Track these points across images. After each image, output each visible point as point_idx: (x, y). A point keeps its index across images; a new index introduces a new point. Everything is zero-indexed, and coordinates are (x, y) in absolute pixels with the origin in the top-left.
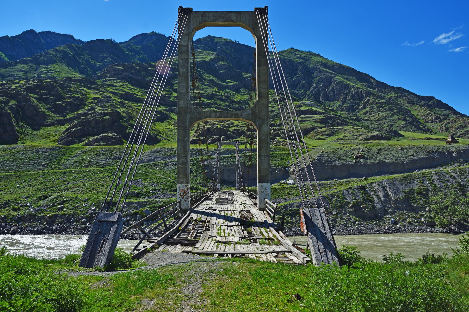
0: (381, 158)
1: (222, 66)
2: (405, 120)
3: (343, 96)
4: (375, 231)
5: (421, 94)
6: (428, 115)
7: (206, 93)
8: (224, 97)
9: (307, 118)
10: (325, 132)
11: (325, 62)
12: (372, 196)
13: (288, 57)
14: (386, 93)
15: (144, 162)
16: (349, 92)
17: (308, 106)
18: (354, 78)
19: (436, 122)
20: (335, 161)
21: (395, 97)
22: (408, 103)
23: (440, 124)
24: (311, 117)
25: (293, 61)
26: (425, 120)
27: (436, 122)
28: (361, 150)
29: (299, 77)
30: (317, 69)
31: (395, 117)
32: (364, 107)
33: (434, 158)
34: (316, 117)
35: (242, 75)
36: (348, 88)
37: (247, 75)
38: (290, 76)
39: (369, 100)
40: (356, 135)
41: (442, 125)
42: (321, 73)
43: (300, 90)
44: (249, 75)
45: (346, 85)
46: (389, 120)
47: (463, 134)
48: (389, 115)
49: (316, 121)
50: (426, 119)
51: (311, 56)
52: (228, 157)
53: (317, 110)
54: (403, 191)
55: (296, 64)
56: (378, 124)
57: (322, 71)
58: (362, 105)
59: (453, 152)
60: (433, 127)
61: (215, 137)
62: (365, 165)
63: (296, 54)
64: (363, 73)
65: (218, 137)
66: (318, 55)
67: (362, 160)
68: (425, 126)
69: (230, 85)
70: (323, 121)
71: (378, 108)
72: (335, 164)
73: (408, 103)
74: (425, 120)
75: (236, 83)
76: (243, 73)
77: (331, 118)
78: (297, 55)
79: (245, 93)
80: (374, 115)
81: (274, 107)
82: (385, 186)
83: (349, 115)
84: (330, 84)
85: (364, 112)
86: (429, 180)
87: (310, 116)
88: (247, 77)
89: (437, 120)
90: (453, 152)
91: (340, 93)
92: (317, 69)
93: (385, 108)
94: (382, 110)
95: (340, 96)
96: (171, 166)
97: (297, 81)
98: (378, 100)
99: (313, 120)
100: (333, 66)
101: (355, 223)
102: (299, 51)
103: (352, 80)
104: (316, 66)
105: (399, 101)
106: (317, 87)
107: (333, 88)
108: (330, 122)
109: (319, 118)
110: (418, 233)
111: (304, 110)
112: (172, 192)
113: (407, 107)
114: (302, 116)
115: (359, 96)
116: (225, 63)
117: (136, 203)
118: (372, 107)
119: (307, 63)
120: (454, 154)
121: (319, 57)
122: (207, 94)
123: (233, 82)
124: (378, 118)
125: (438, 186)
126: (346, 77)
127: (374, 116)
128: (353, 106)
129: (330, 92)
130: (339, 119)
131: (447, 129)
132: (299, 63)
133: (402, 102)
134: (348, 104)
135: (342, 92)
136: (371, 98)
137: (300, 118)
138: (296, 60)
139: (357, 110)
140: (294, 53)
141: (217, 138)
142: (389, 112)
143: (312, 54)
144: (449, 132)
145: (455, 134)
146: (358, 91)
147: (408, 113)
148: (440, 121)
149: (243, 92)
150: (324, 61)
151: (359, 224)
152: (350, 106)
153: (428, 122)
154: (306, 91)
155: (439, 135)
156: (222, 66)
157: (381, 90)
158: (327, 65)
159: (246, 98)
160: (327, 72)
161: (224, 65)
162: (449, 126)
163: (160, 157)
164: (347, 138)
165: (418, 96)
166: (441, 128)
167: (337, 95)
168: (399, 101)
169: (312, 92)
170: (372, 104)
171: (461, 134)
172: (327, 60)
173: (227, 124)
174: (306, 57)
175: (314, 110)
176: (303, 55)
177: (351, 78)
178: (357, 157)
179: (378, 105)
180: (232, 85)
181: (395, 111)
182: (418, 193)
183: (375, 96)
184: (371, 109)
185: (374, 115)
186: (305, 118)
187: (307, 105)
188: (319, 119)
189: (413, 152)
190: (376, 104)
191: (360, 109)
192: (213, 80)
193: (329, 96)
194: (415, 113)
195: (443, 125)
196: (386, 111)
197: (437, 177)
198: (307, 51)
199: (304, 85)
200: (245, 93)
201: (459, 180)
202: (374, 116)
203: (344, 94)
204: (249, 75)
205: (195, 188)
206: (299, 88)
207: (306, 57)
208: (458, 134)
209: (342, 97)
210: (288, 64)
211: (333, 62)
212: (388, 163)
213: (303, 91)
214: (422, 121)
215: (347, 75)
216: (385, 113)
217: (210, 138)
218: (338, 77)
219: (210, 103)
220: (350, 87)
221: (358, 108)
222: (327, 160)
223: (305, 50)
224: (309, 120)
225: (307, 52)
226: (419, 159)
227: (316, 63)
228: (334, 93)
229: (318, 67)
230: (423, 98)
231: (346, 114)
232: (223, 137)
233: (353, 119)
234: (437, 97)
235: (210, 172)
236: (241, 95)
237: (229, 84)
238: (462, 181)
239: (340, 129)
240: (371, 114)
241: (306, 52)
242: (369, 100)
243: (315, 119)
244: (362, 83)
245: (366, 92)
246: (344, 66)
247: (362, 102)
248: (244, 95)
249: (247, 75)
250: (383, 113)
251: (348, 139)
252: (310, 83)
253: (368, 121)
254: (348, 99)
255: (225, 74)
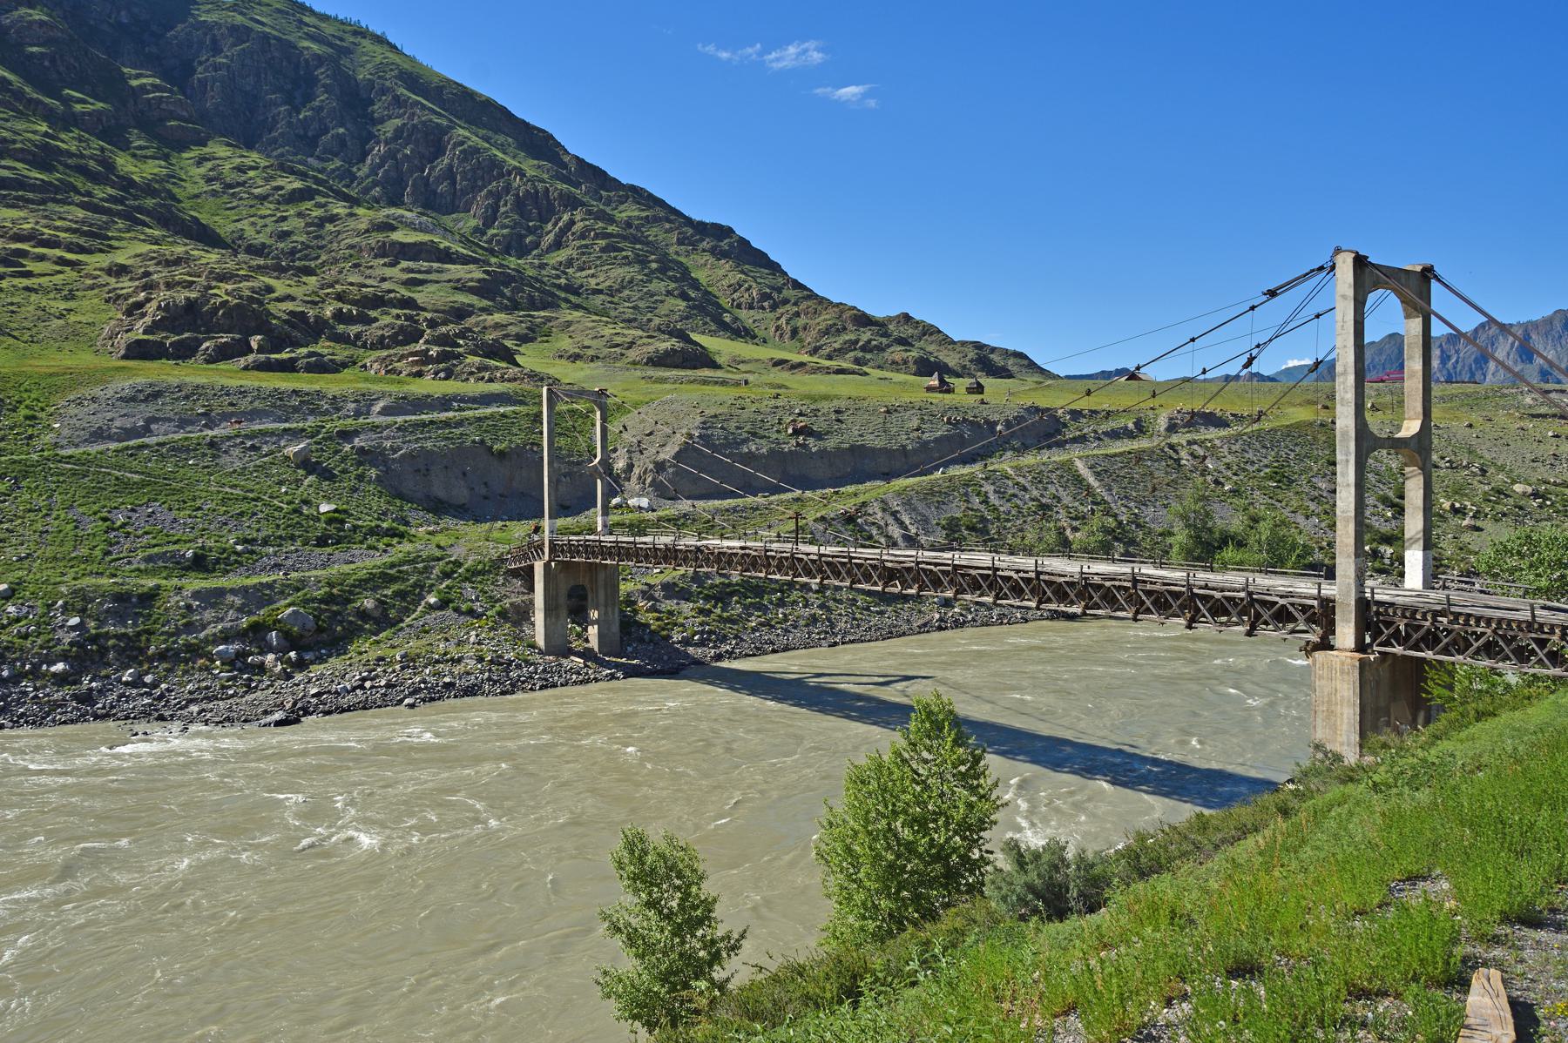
0: (854, 433)
1: (35, 27)
2: (684, 296)
3: (487, 197)
4: (919, 627)
5: (696, 216)
6: (741, 286)
7: (19, 138)
8: (92, 163)
9: (428, 272)
10: (506, 326)
11: (410, 69)
12: (877, 538)
13: (273, 28)
14: (614, 205)
15: (110, 438)
16: (507, 189)
17: (415, 230)
18: (510, 140)
19: (763, 308)
20: (745, 441)
21: (639, 218)
22: (680, 242)
23: (771, 315)
24: (439, 271)
25: (295, 47)
26: (733, 300)
27: (763, 308)
28: (797, 411)
29: (321, 108)
30: (384, 91)
31: (657, 286)
32: (558, 245)
33: (962, 436)
34: (456, 271)
35: (123, 79)
36: (501, 175)
37: (144, 81)
38: (285, 103)
39: (572, 223)
40: (617, 345)
41: (778, 319)
42: (400, 108)
43: (328, 160)
44: (150, 80)
45: (494, 164)
46: (641, 294)
47: (839, 350)
48: (640, 277)
49: (460, 286)
50: (736, 296)
51: (358, 39)
52: (424, 425)
53: (449, 248)
54: (938, 524)
55: (307, 61)
56: (633, 308)
57: (406, 101)
58: (551, 237)
59: (996, 423)
60: (754, 321)
61: (225, 338)
62: (823, 453)
63: (301, 22)
64: (535, 128)
65: (237, 336)
66: (380, 40)
67: (811, 441)
68: (736, 319)
69: (84, 114)
70: (482, 290)
71: (603, 250)
72: (750, 451)
73: (680, 242)
74: (733, 300)
75: (101, 105)
76: (125, 70)
77: (507, 279)
78: (308, 25)
79: (149, 152)
80: (592, 271)
81: (284, 219)
82: (897, 512)
83: (544, 272)
84: (439, 151)
85: (559, 259)
86: (978, 494)
87: (435, 265)
88: (142, 87)
89: (766, 304)
90: (996, 423)
91: (475, 189)
92: (384, 91)
93: (624, 253)
94: (615, 258)
95: (474, 198)
96: (236, 452)
97: (315, 125)
98: (601, 224)
99: (450, 281)
100: (440, 89)
101: (868, 609)
102: (312, 12)
103: (502, 145)
104: (380, 77)
105: (653, 233)
106: (391, 155)
107: (450, 166)
108: (507, 291)
109: (469, 276)
110: (1001, 623)
111: (409, 244)
112: (314, 546)
113: (677, 253)
114: (404, 264)
115: (537, 207)
116: (45, 18)
117: (233, 591)
118: (586, 246)
119: (344, 61)
120: (999, 428)
121: (386, 47)
122: (22, 142)
123: (91, 100)
124: (608, 283)
125: (1002, 509)
126: (482, 132)
127: (593, 276)
128: (523, 237)
129: (439, 180)
130: (532, 286)
131: (794, 332)
132: (320, 60)
133: (660, 238)
134: (506, 227)
135: (480, 183)
136: (578, 215)
137: (403, 270)
138: (306, 44)
139: (535, 252)
140: (293, 15)
141: (233, 339)
142: (637, 267)
143: (362, 33)
144: (801, 341)
145: (820, 347)
146: (535, 188)
147: (685, 275)
148: (774, 308)
149: (140, 148)
150: (406, 66)
151: (878, 613)
152: (510, 235)
153: (739, 306)
154: (351, 164)
155: (775, 347)
156: (35, 27)
157: (596, 192)
158: (415, 79)
159: (156, 170)
160: (424, 107)
161: (42, 23)
162: (801, 322)
163: (169, 420)
164: (590, 352)
165: (689, 221)
166: (778, 328)
167: (464, 192)
168: (653, 233)
169: (374, 171)
170: (583, 236)
171: (835, 350)
172: (412, 60)
173: (253, 290)
174: (341, 39)
175: (442, 246)
176: (328, 29)
177: (501, 139)
178: (796, 432)
179: (602, 243)
180: (89, 114)
181: (654, 266)
182: (968, 528)
183: (589, 213)
184: (583, 253)
185: (592, 271)
186: (420, 272)
187: (411, 226)
188: (471, 280)
189: (915, 423)
190: (597, 236)
191: (545, 248)
192: (10, 83)
193: (435, 192)
194: (701, 275)
195: (783, 320)
196: (629, 264)
197: (992, 488)
198: (340, 17)
199: (342, 141)
200: (149, 152)
201: (1035, 493)
202: (593, 276)
203: (490, 192)
204: (150, 80)
205: (388, 529)
206: (325, 151)
207: (341, 39)
208: (828, 350)
209: (481, 201)
210: (276, 54)
211: (438, 75)
212: (873, 450)
213: (338, 163)
214: (725, 302)
215: (484, 126)
216: (627, 269)
217: (206, 340)
218: (461, 131)
219: (50, 184)
220: (509, 173)
221: (537, 245)
222: (726, 438)
223: (333, 15)
224: (437, 282)
225: (342, 23)
226: (936, 440)
227: (381, 68)
228: (454, 183)
229: (388, 84)
230: (703, 229)
231: (534, 267)
232: (259, 337)
233: (559, 287)
234: (740, 232)
235: (387, 472)
236: (134, 156)
237: (78, 107)
238: (1042, 496)
239: (549, 319)
240: (583, 269)
241: (336, 19)
242: (572, 223)
243: (459, 280)
244: (536, 162)
245: (561, 195)
246: (476, 94)
247: (549, 226)
248: (146, 157)
249: (144, 81)
250: (620, 271)
251: (598, 358)
252: (366, 139)
253: (602, 297)
254: (502, 210)
255: (53, 61)
